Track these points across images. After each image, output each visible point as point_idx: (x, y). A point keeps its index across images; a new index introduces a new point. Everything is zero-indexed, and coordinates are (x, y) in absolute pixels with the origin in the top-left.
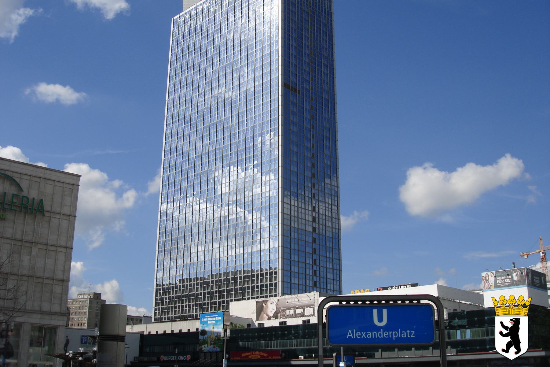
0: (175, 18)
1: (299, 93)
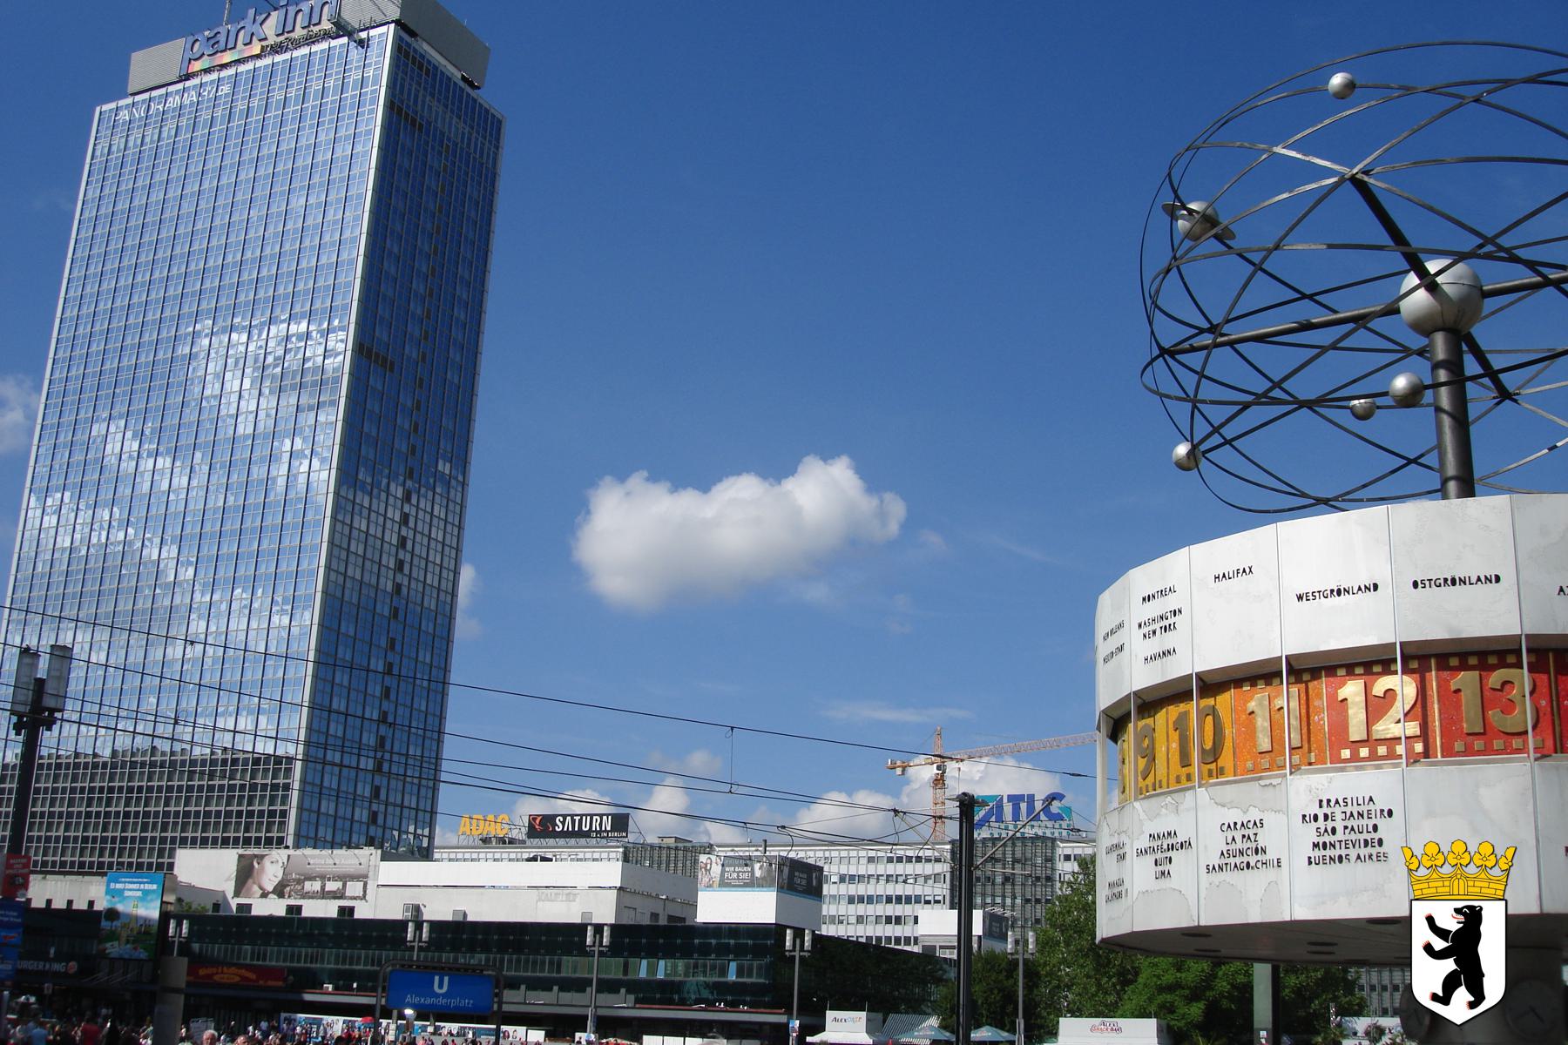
0: (105, 107)
1: (392, 370)
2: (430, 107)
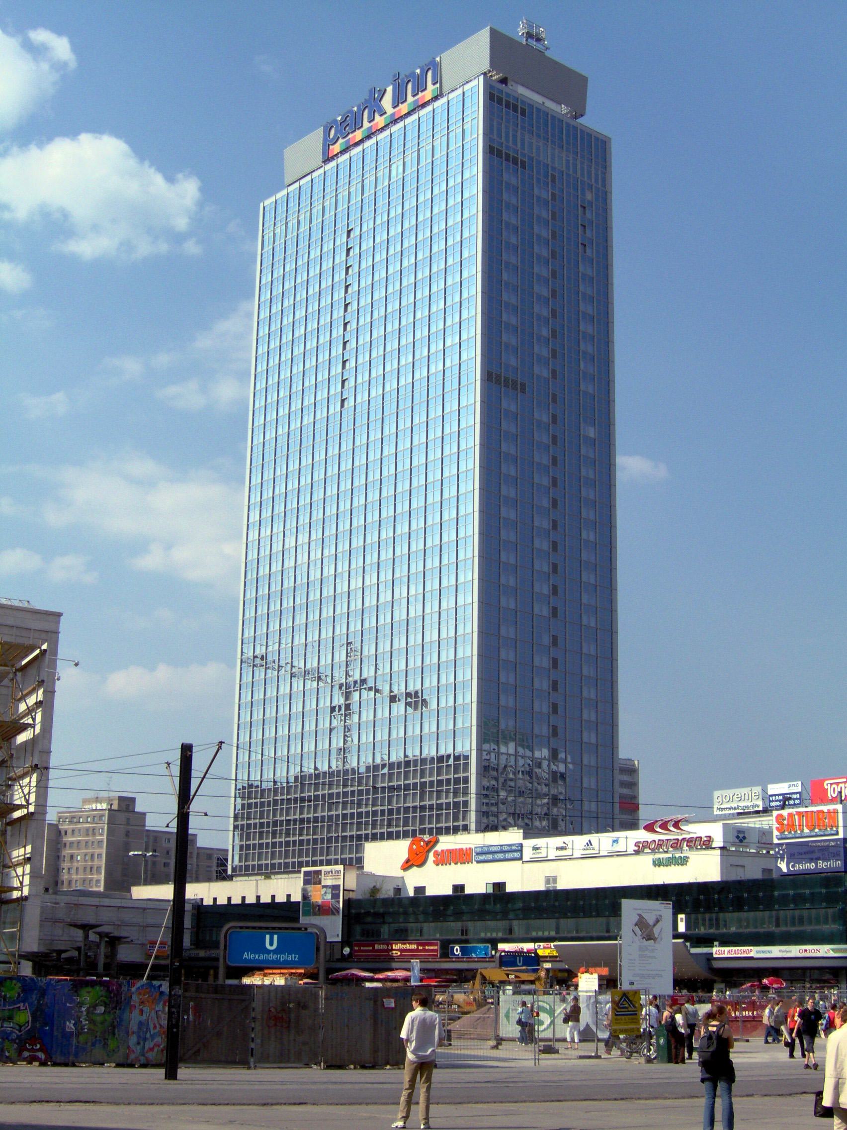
0: (267, 202)
2: (531, 144)
